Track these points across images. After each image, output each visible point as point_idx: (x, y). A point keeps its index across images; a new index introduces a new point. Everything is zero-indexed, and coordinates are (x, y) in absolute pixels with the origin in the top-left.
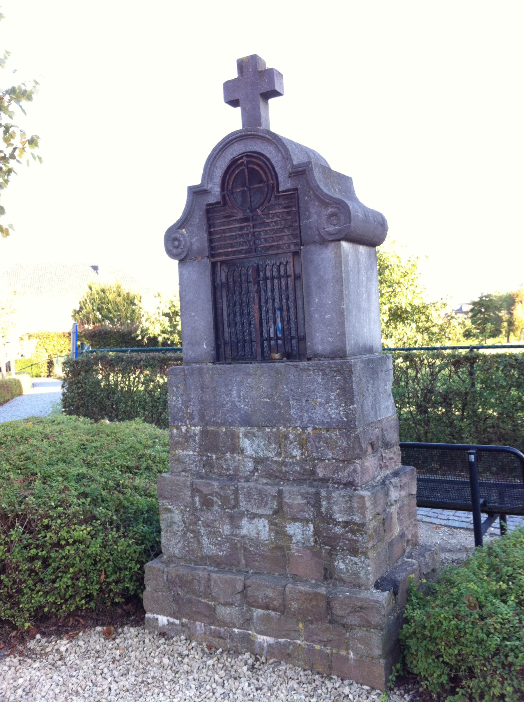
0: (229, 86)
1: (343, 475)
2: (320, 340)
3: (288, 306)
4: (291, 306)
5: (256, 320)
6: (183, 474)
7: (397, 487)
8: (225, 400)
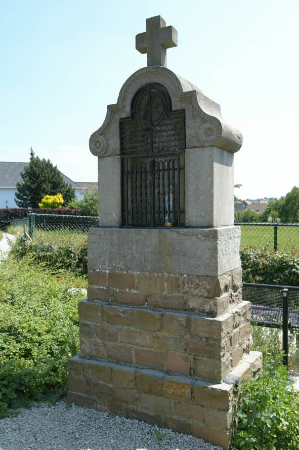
0: (140, 38)
1: (207, 308)
2: (192, 214)
3: (164, 184)
4: (161, 184)
5: (150, 199)
6: (96, 301)
7: (240, 315)
8: (127, 253)
